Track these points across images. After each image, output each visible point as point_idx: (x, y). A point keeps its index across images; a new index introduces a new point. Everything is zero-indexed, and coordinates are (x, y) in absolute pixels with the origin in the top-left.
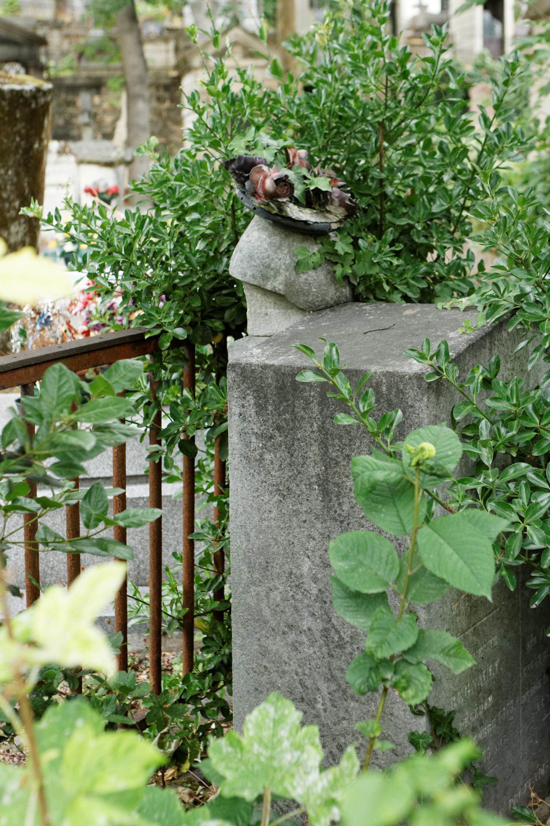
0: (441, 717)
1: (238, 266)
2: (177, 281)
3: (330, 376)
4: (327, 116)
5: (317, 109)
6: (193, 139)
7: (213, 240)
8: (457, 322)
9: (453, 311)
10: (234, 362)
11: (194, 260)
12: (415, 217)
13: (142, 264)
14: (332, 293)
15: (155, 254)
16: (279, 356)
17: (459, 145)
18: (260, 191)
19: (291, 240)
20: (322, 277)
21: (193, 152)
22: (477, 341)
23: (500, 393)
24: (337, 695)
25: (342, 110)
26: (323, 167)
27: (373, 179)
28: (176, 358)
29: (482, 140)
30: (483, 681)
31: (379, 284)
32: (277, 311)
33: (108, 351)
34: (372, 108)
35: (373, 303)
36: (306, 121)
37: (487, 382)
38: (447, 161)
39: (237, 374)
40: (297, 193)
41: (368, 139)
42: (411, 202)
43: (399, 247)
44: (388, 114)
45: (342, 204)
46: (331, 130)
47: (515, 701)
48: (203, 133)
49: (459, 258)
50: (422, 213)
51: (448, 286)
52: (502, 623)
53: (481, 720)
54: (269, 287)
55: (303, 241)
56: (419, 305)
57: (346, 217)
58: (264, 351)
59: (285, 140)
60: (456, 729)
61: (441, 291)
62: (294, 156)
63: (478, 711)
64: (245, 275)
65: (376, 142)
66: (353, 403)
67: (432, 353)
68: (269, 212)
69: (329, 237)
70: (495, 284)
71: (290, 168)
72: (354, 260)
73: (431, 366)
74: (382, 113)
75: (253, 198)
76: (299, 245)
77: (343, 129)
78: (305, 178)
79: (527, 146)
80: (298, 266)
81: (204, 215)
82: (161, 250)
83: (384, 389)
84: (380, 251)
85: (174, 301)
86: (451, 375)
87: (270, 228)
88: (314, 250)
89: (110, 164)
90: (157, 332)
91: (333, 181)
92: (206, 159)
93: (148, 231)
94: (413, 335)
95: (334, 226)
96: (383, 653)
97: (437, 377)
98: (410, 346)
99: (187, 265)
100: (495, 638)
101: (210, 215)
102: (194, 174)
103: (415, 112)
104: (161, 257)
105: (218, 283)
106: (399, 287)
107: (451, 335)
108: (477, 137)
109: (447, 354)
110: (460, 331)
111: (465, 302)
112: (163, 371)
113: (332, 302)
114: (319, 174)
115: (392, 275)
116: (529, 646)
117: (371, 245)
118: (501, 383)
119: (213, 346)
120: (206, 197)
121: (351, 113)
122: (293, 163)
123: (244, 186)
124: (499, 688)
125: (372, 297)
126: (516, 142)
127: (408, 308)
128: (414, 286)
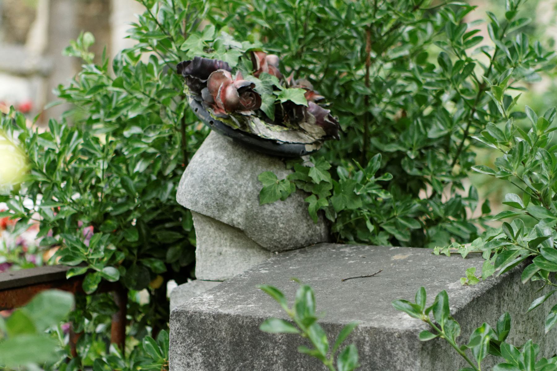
1: (187, 192)
2: (110, 209)
3: (302, 327)
4: (303, 18)
5: (292, 9)
6: (138, 36)
7: (156, 162)
8: (459, 272)
9: (453, 258)
10: (180, 309)
11: (133, 183)
12: (407, 143)
13: (67, 185)
14: (302, 231)
15: (83, 177)
16: (236, 304)
17: (463, 58)
18: (220, 101)
19: (254, 163)
20: (291, 210)
21: (137, 52)
22: (483, 295)
23: (511, 359)
25: (321, 10)
26: (296, 78)
27: (356, 95)
28: (104, 305)
29: (492, 53)
31: (361, 222)
32: (234, 250)
33: (19, 291)
34: (358, 9)
35: (353, 245)
36: (277, 23)
37: (494, 346)
38: (448, 76)
39: (183, 325)
40: (264, 106)
41: (352, 47)
42: (400, 127)
43: (388, 177)
44: (378, 17)
45: (320, 121)
46: (306, 33)
48: (151, 29)
49: (458, 196)
50: (416, 138)
51: (445, 230)
54: (225, 219)
55: (270, 164)
57: (325, 138)
58: (217, 297)
59: (252, 43)
61: (437, 235)
62: (262, 62)
64: (196, 203)
65: (362, 50)
66: (331, 362)
67: (427, 307)
68: (230, 128)
69: (302, 161)
70: (507, 225)
71: (257, 76)
72: (331, 191)
73: (426, 321)
74: (370, 16)
75: (210, 110)
76: (264, 169)
77: (322, 33)
78: (275, 88)
79: (546, 63)
80: (263, 195)
81: (147, 129)
82: (91, 170)
83: (367, 348)
84: (364, 181)
85: (104, 234)
86: (450, 333)
87: (230, 147)
88: (283, 176)
89: (23, 75)
90: (82, 271)
91: (309, 94)
92: (152, 62)
93: (76, 148)
94: (403, 284)
95: (309, 148)
97: (434, 336)
98: (400, 297)
99: (123, 191)
101: (155, 129)
102: (137, 79)
103: (412, 16)
104: (91, 178)
105: (159, 215)
106: (386, 228)
107: (451, 286)
108: (486, 50)
109: (446, 307)
110: (462, 281)
111: (468, 248)
112: (86, 321)
113: (303, 242)
114: (291, 84)
115: (378, 212)
117: (352, 174)
118: (512, 347)
119: (149, 291)
120: (151, 107)
121: (332, 15)
122: (261, 70)
123: (200, 94)
125: (352, 238)
126: (531, 58)
127: (397, 252)
128: (404, 226)
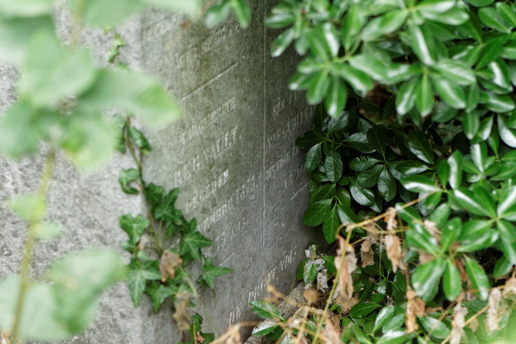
0: (160, 196)
24: (30, 171)
30: (216, 152)
47: (256, 177)
52: (241, 81)
53: (214, 200)
56: (460, 283)
60: (180, 211)
63: (210, 189)
96: (47, 98)
100: (233, 100)
116: (275, 112)
124: (237, 161)
